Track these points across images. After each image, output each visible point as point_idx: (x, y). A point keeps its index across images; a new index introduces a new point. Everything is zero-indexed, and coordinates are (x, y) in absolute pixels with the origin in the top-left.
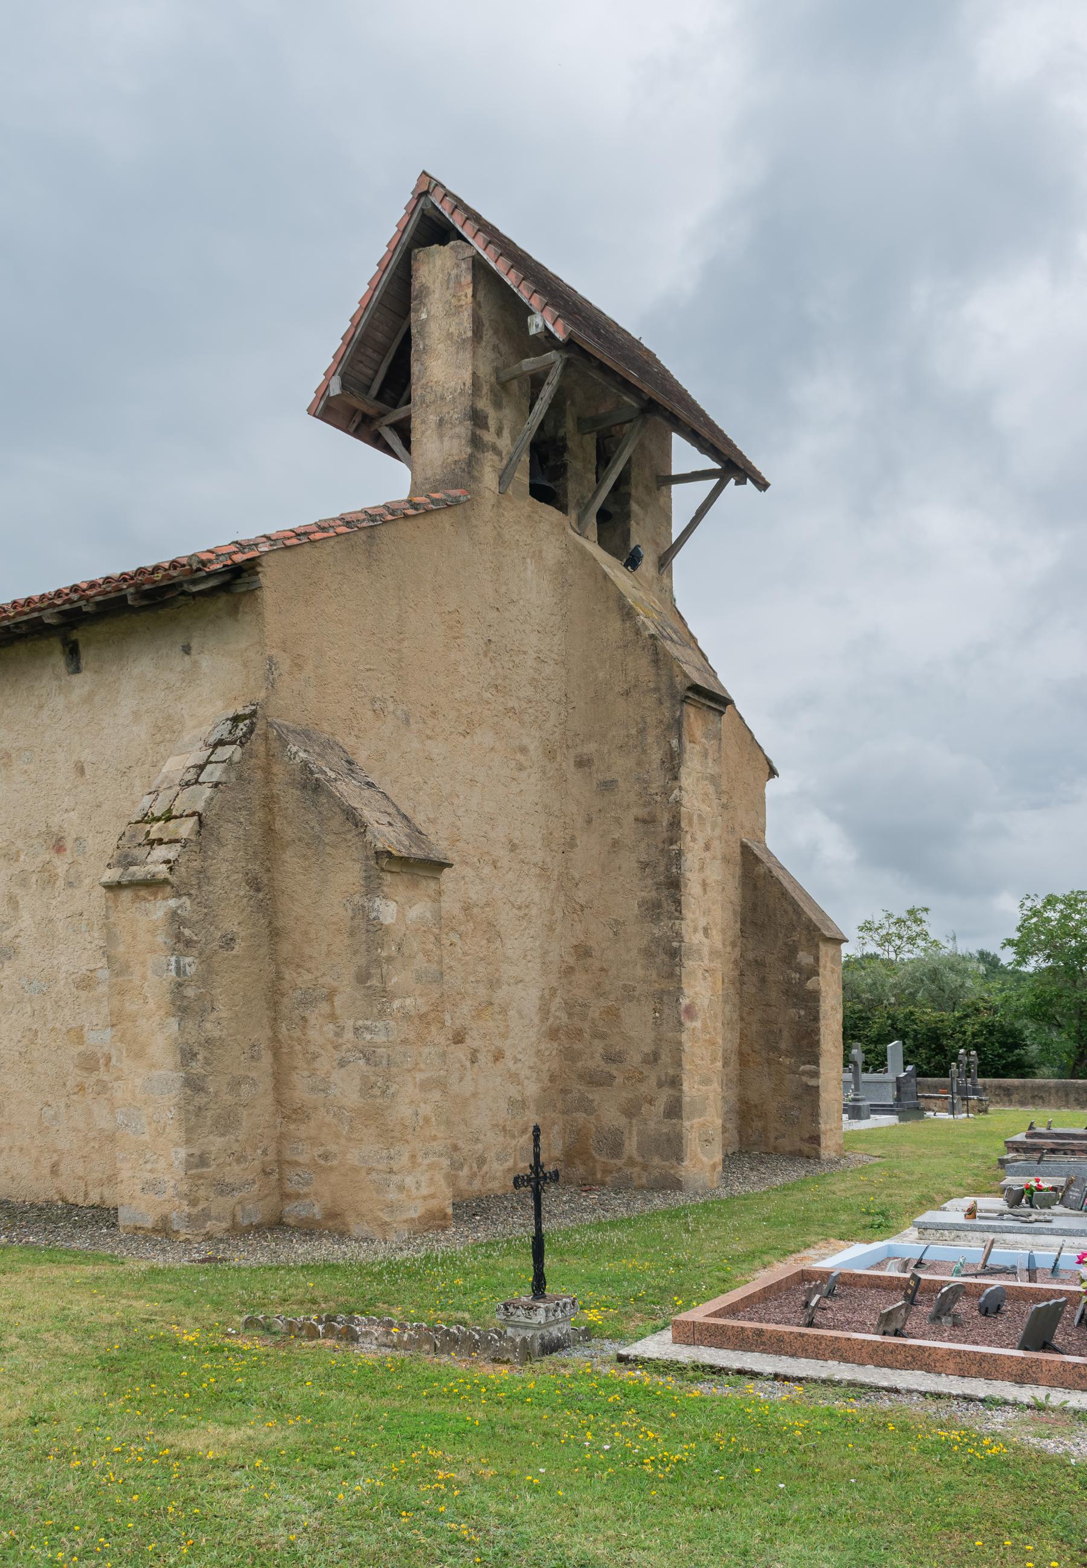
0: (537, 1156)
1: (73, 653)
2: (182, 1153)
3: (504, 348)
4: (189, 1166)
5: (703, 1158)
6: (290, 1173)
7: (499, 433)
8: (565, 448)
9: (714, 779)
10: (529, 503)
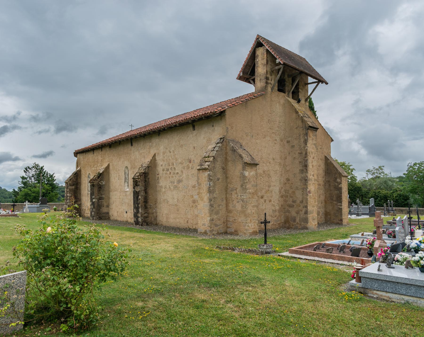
0: (265, 218)
1: (194, 127)
2: (209, 218)
3: (272, 65)
4: (210, 221)
5: (313, 223)
6: (228, 223)
7: (271, 80)
8: (285, 81)
9: (315, 144)
10: (277, 93)
